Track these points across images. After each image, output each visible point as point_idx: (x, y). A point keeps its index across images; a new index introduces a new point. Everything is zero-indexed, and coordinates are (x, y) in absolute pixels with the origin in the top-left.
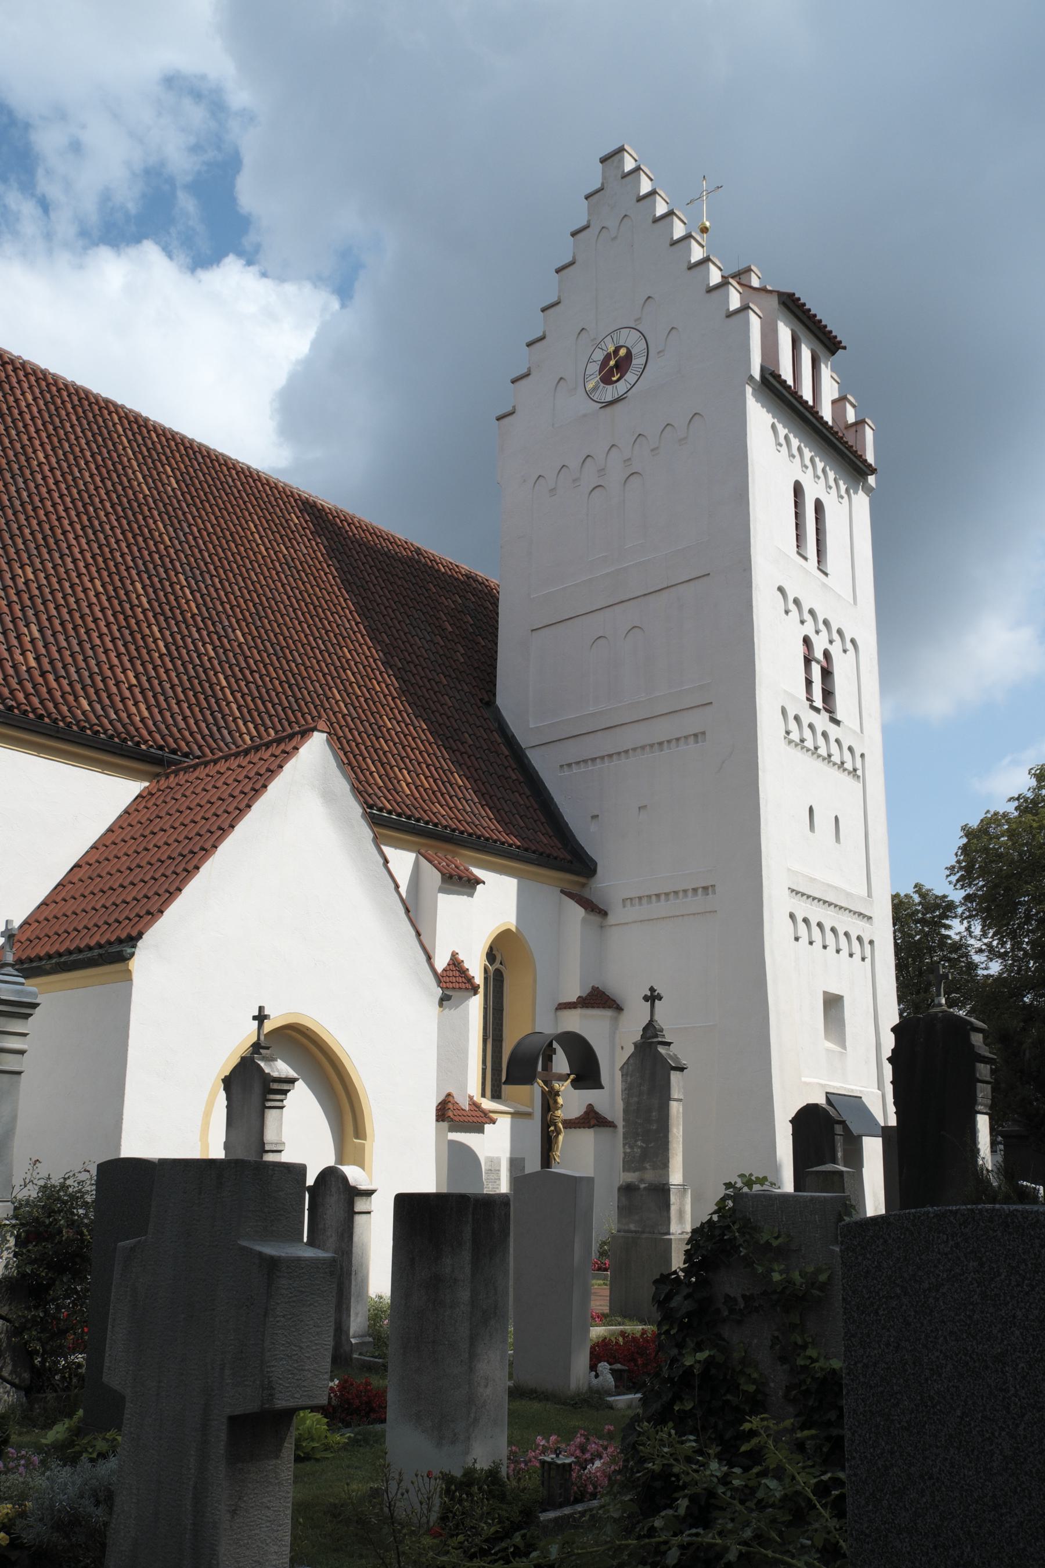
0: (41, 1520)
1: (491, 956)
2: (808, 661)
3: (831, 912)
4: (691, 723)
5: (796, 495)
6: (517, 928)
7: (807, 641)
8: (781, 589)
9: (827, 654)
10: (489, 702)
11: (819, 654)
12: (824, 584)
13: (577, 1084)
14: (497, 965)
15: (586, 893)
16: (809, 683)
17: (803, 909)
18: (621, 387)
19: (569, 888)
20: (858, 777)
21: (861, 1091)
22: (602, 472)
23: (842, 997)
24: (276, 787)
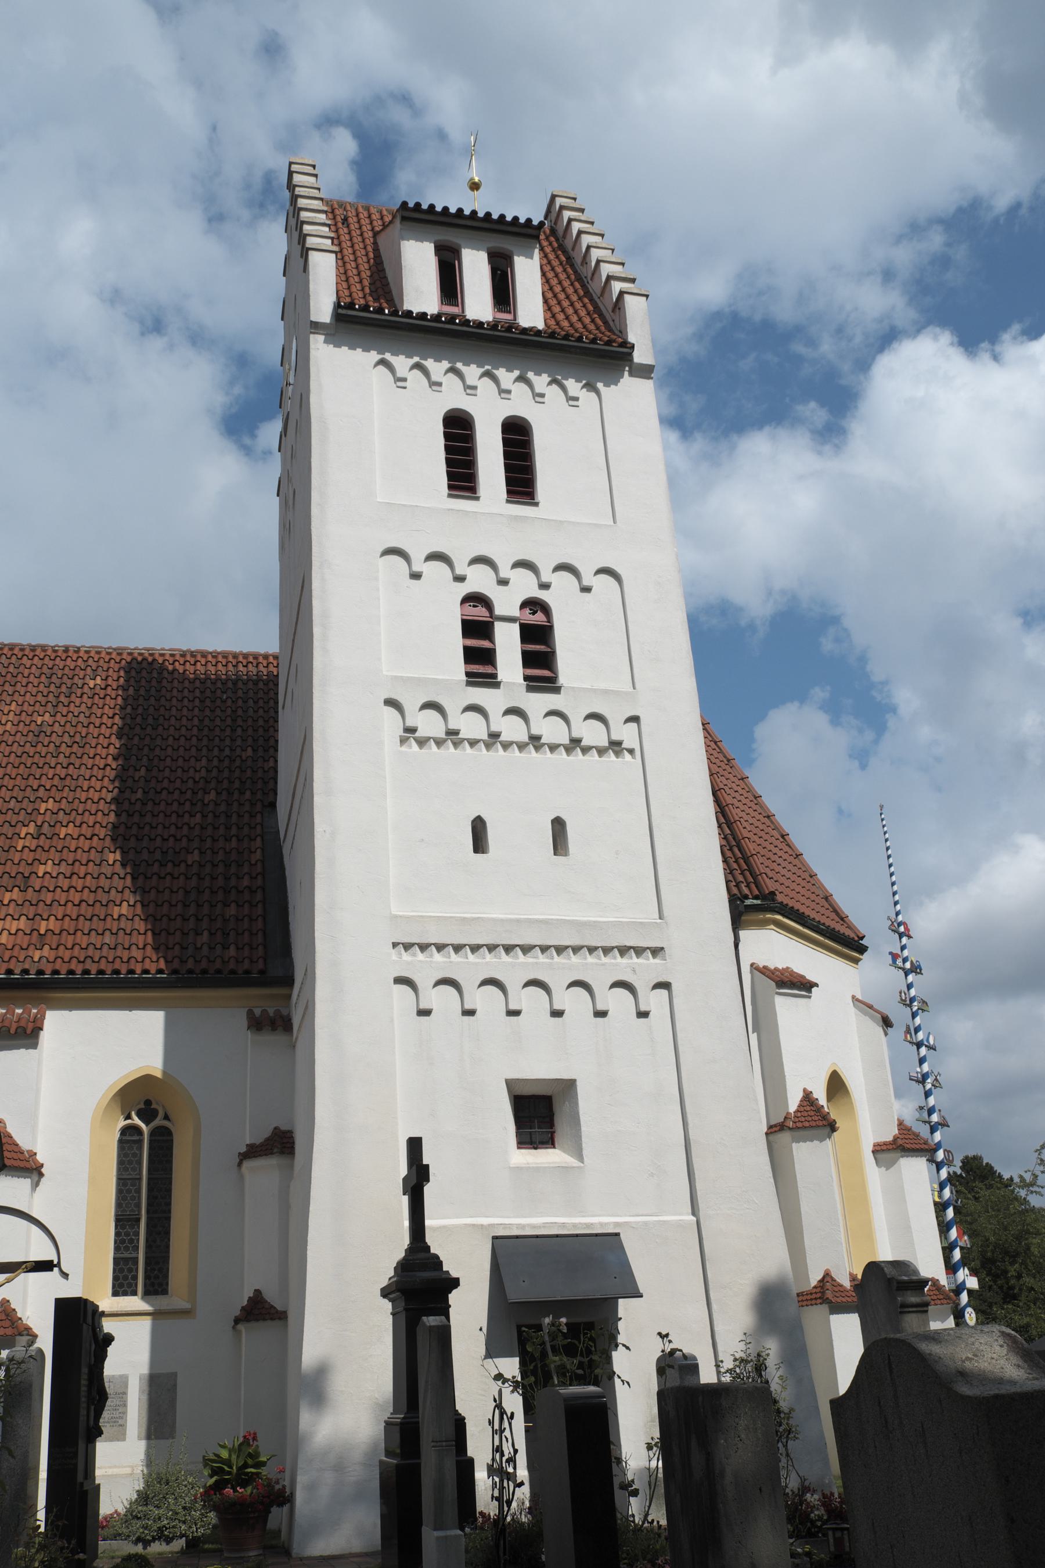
6: (164, 1073)
14: (158, 1122)
17: (425, 968)
20: (631, 751)
21: (617, 1224)
23: (575, 1081)
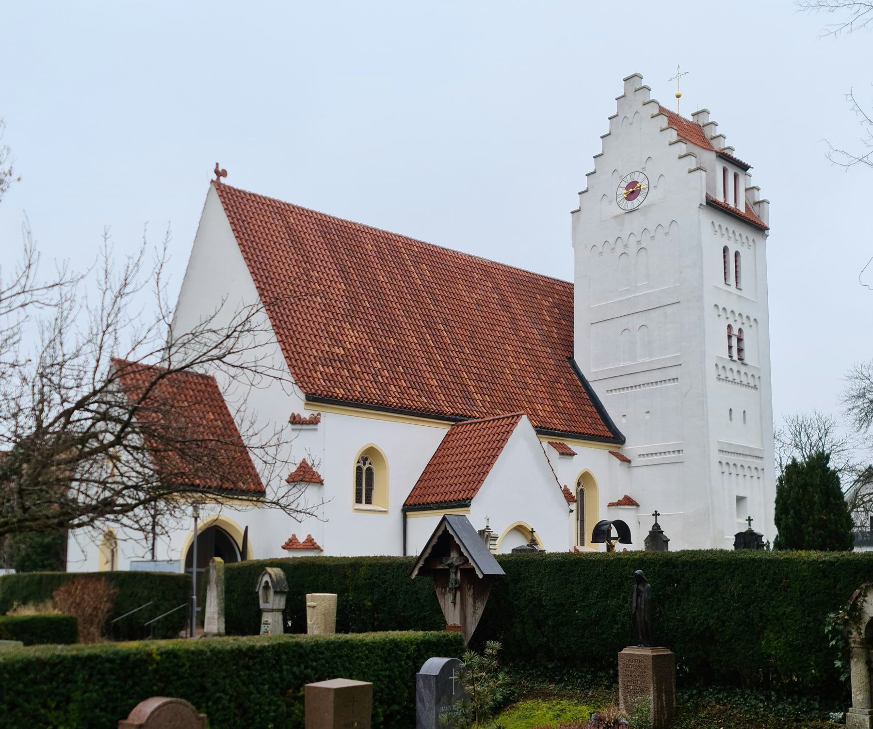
0: (775, 573)
1: (579, 484)
2: (730, 337)
3: (741, 458)
4: (672, 373)
5: (724, 252)
7: (729, 327)
8: (716, 305)
9: (740, 330)
10: (571, 359)
11: (735, 332)
12: (739, 296)
13: (621, 542)
15: (620, 452)
16: (730, 347)
17: (725, 458)
18: (636, 203)
19: (612, 450)
22: (626, 246)
24: (512, 439)
